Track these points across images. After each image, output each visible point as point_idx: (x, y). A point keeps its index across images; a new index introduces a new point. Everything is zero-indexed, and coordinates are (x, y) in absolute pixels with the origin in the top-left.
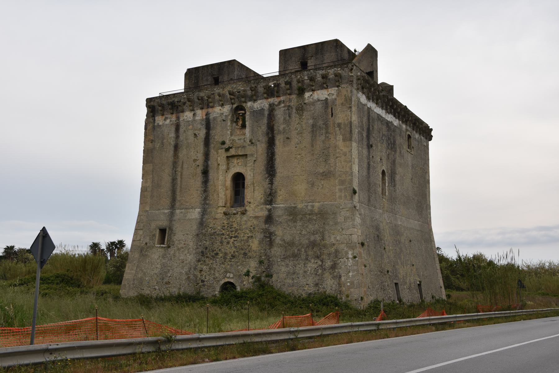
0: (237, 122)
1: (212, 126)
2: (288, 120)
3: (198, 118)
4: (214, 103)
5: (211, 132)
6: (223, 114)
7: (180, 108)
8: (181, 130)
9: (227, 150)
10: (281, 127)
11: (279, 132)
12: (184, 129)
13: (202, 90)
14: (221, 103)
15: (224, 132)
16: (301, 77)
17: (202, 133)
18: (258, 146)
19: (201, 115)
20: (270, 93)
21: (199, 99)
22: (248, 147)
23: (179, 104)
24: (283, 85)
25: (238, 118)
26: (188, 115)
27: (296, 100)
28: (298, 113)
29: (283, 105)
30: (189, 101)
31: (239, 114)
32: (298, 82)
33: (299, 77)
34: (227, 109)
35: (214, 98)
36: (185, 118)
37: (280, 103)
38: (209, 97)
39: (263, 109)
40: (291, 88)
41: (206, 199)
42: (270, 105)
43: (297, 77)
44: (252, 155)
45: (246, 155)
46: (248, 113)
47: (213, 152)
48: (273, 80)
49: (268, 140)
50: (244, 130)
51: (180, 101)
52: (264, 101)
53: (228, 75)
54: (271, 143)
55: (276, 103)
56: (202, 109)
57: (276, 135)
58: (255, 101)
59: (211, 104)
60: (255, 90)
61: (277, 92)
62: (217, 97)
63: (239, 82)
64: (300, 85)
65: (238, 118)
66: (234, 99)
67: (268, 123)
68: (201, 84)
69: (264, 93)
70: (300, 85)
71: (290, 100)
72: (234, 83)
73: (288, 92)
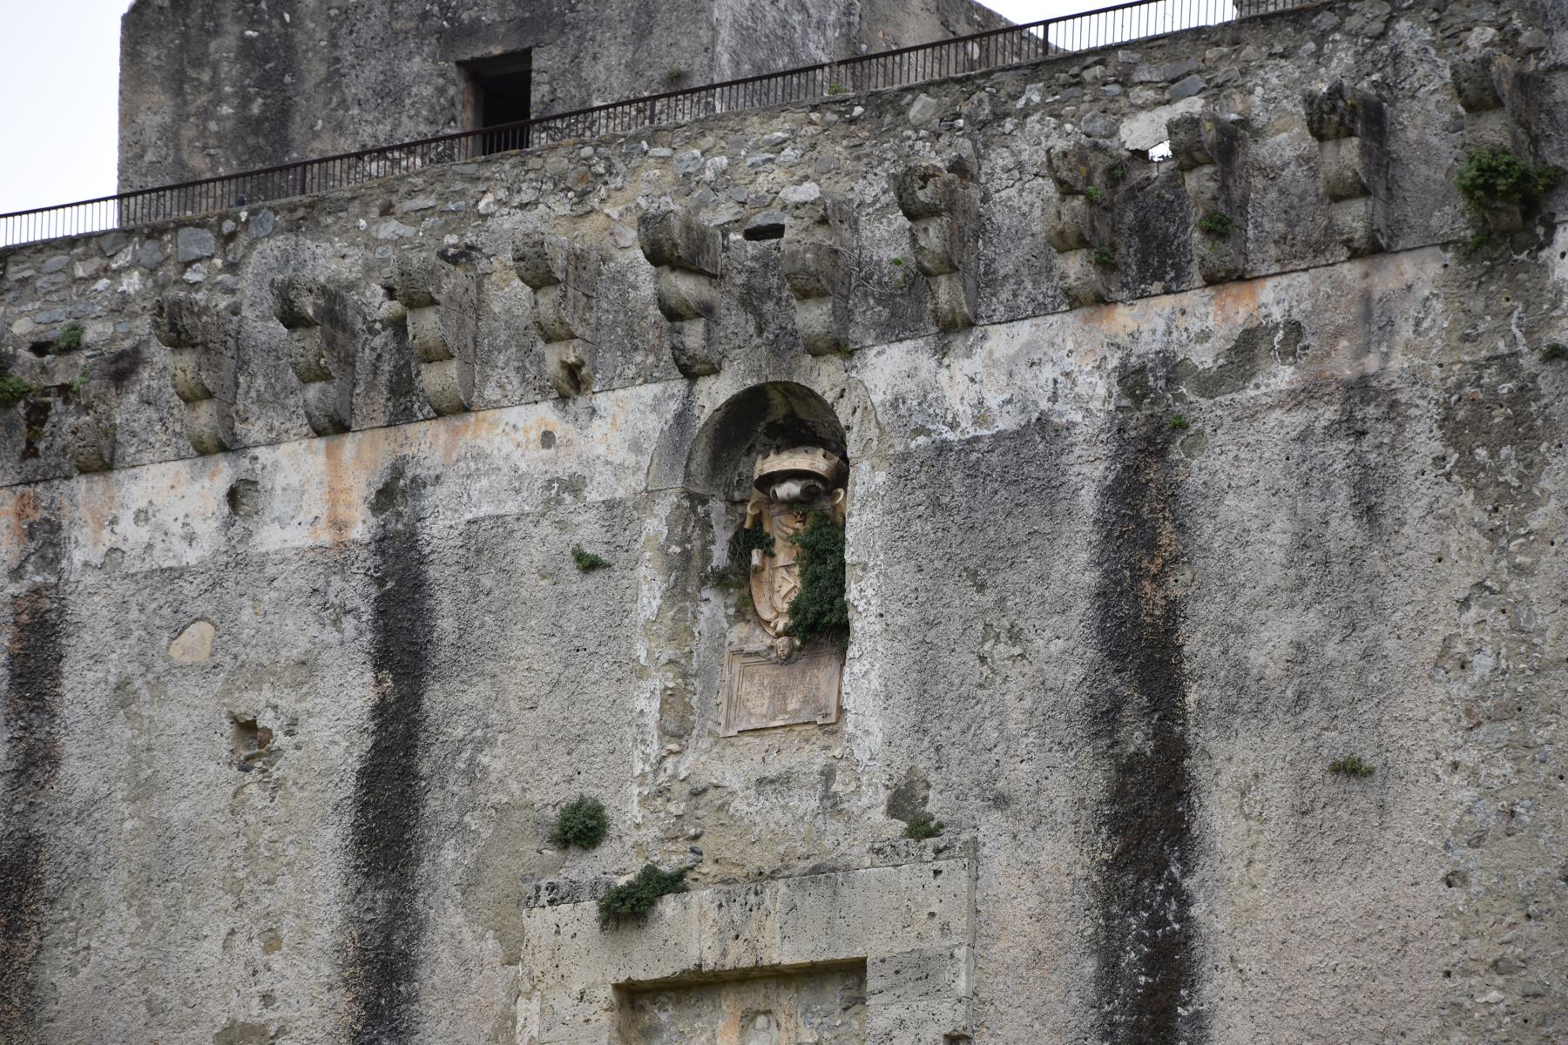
0: (737, 579)
1: (446, 625)
2: (1354, 559)
3: (282, 534)
4: (476, 355)
5: (435, 698)
6: (574, 486)
7: (66, 421)
8: (82, 683)
9: (628, 908)
10: (1270, 643)
11: (1246, 697)
12: (114, 668)
13: (340, 206)
14: (554, 357)
15: (598, 691)
16: (1508, 39)
17: (334, 716)
18: (998, 858)
19: (315, 503)
20: (1131, 233)
21: (293, 319)
22: (871, 873)
23: (63, 371)
24: (1285, 142)
25: (751, 539)
26: (160, 503)
27: (1440, 316)
28: (1469, 468)
29: (1282, 376)
30: (178, 339)
31: (765, 476)
32: (1477, 95)
33: (1479, 38)
34: (626, 429)
35: (479, 308)
36: (131, 533)
37: (1247, 349)
38: (412, 294)
39: (1044, 430)
40: (1379, 176)
41: (712, 984)
42: (1133, 382)
43: (1453, 38)
44: (922, 971)
45: (854, 970)
46: (867, 477)
47: (453, 938)
48: (1170, 89)
49: (1118, 794)
50: (821, 676)
51: (72, 345)
52: (1065, 327)
53: (642, 34)
54: (1149, 823)
55: (1204, 358)
56: (333, 426)
57: (1202, 736)
58: (953, 329)
59: (436, 379)
60: (947, 206)
61: (1219, 229)
62: (510, 295)
63: (771, 112)
64: (1494, 130)
65: (751, 539)
66: (706, 311)
67: (1103, 596)
68: (316, 138)
69: (1063, 242)
70: (1494, 130)
71: (1374, 320)
72: (703, 126)
73: (1353, 217)
